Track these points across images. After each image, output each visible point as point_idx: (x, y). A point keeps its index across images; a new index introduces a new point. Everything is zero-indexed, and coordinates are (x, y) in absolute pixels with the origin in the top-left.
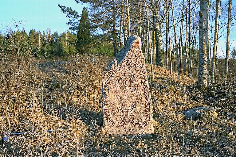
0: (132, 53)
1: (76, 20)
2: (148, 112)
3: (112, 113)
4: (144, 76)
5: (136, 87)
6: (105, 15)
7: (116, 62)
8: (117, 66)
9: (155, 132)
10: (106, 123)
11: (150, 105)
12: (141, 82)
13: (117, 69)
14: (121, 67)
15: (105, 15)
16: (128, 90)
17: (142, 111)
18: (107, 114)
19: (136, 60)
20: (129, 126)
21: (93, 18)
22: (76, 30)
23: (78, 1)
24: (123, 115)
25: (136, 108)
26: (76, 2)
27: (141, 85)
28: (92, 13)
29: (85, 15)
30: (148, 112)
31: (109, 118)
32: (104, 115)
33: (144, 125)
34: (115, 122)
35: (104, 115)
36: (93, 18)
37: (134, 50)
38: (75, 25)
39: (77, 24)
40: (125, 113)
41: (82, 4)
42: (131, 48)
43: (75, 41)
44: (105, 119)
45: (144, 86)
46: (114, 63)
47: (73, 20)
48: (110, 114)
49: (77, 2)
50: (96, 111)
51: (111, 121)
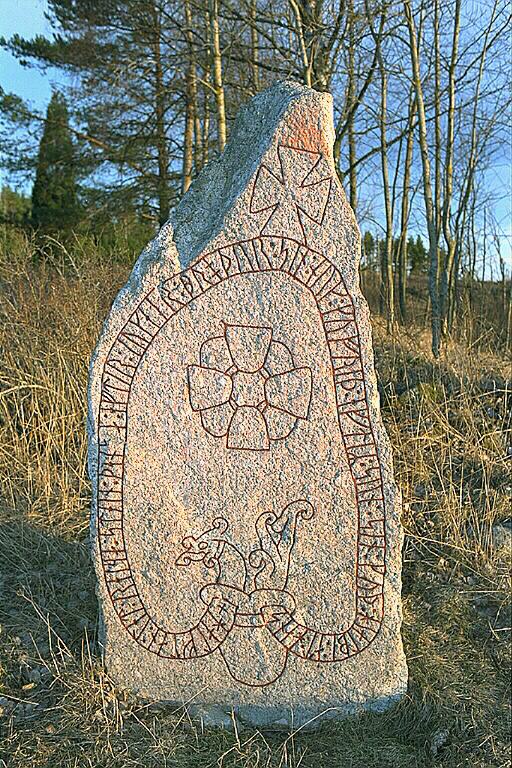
0: (272, 191)
1: (21, 133)
2: (374, 567)
3: (152, 575)
4: (353, 342)
5: (300, 413)
6: (127, 116)
7: (171, 252)
8: (177, 280)
9: (414, 687)
10: (115, 632)
11: (391, 522)
12: (331, 379)
13: (176, 295)
14: (205, 286)
15: (127, 116)
16: (248, 427)
17: (338, 562)
18: (120, 575)
19: (300, 238)
20: (256, 646)
21: (86, 125)
22: (22, 169)
23: (28, 59)
24: (218, 582)
25: (299, 545)
26: (21, 63)
27: (331, 397)
28: (80, 105)
29: (57, 113)
30: (374, 567)
31: (131, 601)
32: (103, 583)
33: (351, 644)
34: (170, 626)
35: (103, 583)
36: (86, 125)
37: (289, 172)
38: (16, 150)
39: (24, 148)
40: (229, 573)
41: (42, 71)
42: (270, 156)
43: (25, 215)
44: (107, 607)
45: (354, 402)
46: (158, 257)
47: (8, 132)
48: (140, 581)
49: (24, 63)
50: (226, 219)
51: (142, 623)
